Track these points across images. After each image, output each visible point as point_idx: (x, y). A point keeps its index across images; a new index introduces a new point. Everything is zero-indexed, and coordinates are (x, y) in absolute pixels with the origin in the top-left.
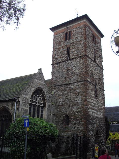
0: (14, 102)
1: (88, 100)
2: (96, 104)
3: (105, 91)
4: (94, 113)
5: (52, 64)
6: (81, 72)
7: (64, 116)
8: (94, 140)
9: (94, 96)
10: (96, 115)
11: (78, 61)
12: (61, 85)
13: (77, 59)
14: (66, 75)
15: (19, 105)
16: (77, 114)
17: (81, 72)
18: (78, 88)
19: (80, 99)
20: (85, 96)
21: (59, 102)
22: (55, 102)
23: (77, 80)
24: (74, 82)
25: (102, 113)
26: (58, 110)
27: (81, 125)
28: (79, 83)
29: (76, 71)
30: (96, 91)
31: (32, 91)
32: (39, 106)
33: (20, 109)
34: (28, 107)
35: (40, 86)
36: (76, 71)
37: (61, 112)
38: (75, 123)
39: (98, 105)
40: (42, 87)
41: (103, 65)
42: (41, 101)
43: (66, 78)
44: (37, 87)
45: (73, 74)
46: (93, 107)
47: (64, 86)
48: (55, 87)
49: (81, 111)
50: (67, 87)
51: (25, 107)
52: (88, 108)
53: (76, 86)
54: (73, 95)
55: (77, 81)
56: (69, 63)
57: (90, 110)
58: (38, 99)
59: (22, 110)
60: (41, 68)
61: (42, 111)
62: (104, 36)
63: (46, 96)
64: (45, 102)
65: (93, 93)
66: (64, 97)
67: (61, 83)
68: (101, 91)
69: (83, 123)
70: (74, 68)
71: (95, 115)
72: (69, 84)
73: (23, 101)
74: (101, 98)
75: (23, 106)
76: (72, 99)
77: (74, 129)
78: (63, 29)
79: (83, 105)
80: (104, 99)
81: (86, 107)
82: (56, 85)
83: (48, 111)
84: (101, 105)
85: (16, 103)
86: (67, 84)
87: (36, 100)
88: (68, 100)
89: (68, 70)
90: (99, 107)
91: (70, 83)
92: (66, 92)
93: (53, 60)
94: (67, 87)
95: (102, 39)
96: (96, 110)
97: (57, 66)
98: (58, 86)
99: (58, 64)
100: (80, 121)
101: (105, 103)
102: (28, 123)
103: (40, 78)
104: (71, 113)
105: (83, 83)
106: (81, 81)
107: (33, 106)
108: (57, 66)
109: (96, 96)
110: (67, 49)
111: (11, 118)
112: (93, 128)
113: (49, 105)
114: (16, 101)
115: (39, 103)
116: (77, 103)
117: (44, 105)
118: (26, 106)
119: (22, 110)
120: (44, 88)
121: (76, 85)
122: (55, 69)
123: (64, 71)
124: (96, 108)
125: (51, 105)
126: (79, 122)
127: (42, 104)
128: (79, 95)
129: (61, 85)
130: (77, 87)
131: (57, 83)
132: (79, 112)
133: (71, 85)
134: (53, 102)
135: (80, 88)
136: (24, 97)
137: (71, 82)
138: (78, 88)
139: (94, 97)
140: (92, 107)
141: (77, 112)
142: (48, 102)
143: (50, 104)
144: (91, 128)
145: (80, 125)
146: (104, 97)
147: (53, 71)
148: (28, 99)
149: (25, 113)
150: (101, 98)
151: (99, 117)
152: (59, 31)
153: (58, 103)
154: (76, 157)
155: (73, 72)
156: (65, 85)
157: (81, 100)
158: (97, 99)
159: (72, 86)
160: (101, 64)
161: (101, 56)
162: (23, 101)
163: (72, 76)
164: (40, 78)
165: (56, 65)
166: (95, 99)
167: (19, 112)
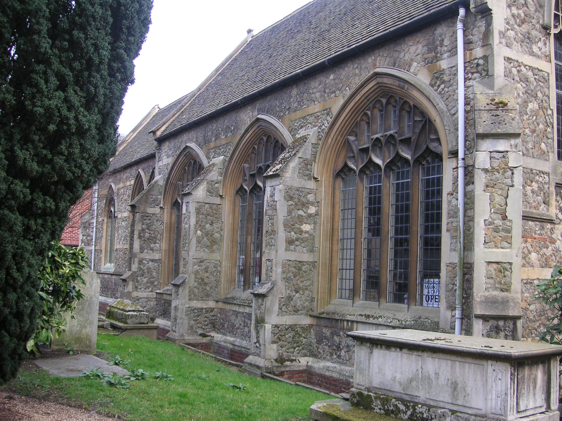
0: (441, 30)
15: (487, 35)
51: (532, 54)
59: (514, 71)
85: (460, 25)
111: (433, 146)
114: (462, 12)
118: (535, 49)
119: (514, 71)
149: (536, 97)
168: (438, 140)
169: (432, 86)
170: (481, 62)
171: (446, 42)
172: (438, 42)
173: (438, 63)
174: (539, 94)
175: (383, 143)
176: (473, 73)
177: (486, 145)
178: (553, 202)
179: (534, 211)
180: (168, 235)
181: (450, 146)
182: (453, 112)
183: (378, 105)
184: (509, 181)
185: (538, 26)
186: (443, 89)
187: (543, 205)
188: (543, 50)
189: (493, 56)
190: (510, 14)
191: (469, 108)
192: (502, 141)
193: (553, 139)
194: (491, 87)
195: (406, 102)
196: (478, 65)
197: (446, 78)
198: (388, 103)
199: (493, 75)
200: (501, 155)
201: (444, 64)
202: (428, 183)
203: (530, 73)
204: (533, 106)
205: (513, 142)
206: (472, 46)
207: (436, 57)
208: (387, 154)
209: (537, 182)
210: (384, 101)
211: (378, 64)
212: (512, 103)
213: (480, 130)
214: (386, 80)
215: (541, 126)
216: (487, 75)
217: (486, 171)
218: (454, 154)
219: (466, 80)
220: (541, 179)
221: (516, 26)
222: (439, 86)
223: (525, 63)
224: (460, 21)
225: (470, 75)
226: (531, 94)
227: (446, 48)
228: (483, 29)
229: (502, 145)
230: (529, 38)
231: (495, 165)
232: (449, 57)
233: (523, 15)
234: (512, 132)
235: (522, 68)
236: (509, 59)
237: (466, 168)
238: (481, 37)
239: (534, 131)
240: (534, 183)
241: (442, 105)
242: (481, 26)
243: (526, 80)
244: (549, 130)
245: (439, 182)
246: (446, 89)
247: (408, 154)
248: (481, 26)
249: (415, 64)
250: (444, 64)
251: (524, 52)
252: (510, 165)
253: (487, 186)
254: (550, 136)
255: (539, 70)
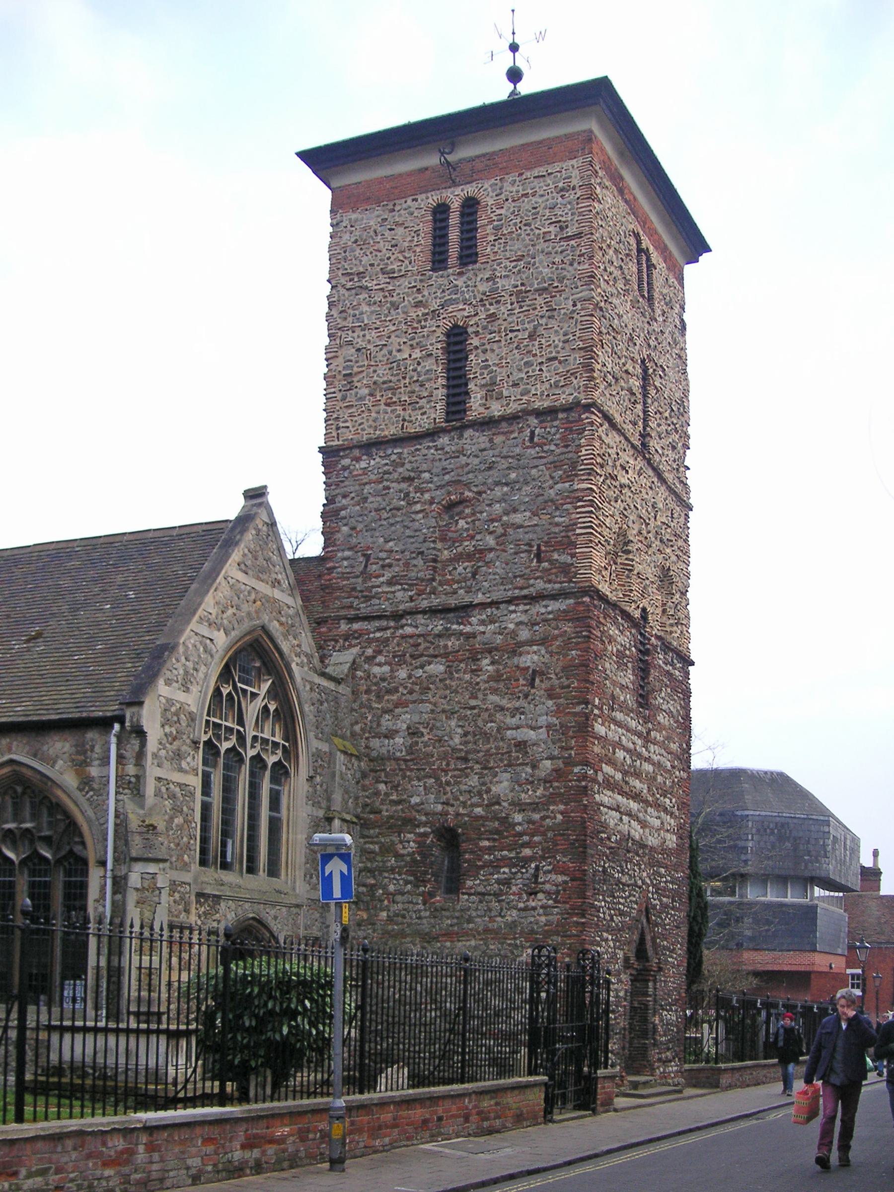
0: (91, 735)
1: (600, 729)
2: (639, 756)
3: (692, 663)
4: (629, 814)
5: (321, 450)
6: (557, 530)
7: (425, 835)
8: (622, 994)
9: (628, 698)
10: (637, 832)
11: (534, 445)
12: (402, 617)
13: (528, 432)
14: (439, 545)
15: (140, 755)
16: (518, 818)
17: (557, 530)
18: (530, 643)
19: (543, 720)
20: (579, 704)
21: (390, 735)
22: (353, 734)
23: (520, 582)
24: (495, 596)
25: (672, 814)
26: (377, 793)
27: (548, 893)
28: (539, 608)
29: (517, 518)
30: (643, 669)
31: (217, 657)
32: (258, 760)
33: (150, 788)
34: (195, 771)
35: (265, 618)
36: (517, 518)
37: (399, 802)
38: (507, 882)
39: (648, 760)
40: (275, 627)
41: (692, 478)
42: (268, 727)
43: (435, 561)
44: (246, 626)
45: (491, 541)
46: (625, 773)
47: (421, 619)
48: (356, 626)
49: (552, 799)
50: (447, 629)
51: (181, 770)
52: (595, 780)
53: (518, 624)
54: (495, 691)
55: (525, 592)
56: (461, 452)
57: (605, 797)
58: (252, 710)
59: (163, 789)
60: (265, 487)
61: (275, 803)
62: (708, 249)
63: (301, 688)
64: (290, 734)
65: (628, 677)
66: (422, 701)
67: (399, 595)
68: (672, 664)
69: (560, 878)
70: (498, 492)
71: (633, 832)
72: (464, 610)
73: (167, 729)
74: (670, 714)
75: (167, 764)
76: (485, 715)
77: (499, 919)
78: (410, 174)
79: (566, 764)
80: (687, 718)
81: (585, 777)
82: (364, 609)
83: (313, 800)
84: (669, 767)
85: (114, 740)
86: (444, 611)
87: (241, 722)
88: (453, 723)
89: (450, 507)
90: (655, 779)
91: (471, 606)
92: (437, 668)
93: (332, 419)
94: (446, 634)
95: (689, 271)
96: (636, 796)
97: (363, 464)
98: (379, 618)
99: (370, 456)
100: (537, 868)
101: (689, 747)
102: (345, 879)
103: (261, 561)
104: (479, 810)
105: (564, 611)
106: (554, 597)
107: (221, 761)
108: (363, 464)
109: (644, 699)
110: (448, 344)
111: (77, 849)
112: (622, 913)
113: (318, 755)
114: (117, 727)
115: (255, 738)
116: (522, 745)
117: (290, 753)
118: (184, 765)
119: (163, 789)
120: (285, 636)
121: (514, 617)
122: (351, 487)
123: (418, 507)
124: (637, 784)
125: (331, 754)
126: (536, 876)
127: (276, 745)
128: (538, 694)
129: (397, 616)
130: (524, 634)
131: (368, 598)
132: (535, 806)
133: (474, 620)
134: (343, 737)
135: (544, 641)
136: (170, 702)
137: (480, 598)
138: (530, 643)
139: (628, 711)
140: (619, 776)
141: (521, 807)
142: (311, 735)
143: (325, 747)
144: (611, 916)
145: (540, 896)
146: (687, 708)
147: (330, 500)
148: (192, 718)
149: (181, 812)
150: (670, 714)
151: (652, 841)
152: (380, 181)
153: (375, 743)
154: (546, 1084)
155: (493, 521)
156: (433, 612)
157: (549, 727)
158: (647, 720)
159: (482, 623)
160: (681, 467)
161: (681, 408)
162: (167, 729)
163: (481, 552)
164: (261, 561)
165: (358, 459)
166: (633, 724)
167: (142, 807)
168: (83, 843)
169: (81, 790)
170: (133, 780)
171: (97, 749)
172: (88, 747)
173: (88, 768)
174: (185, 809)
175: (18, 837)
176: (124, 789)
177: (138, 867)
178: (193, 911)
179: (176, 919)
180: (94, 995)
181: (98, 854)
182: (102, 821)
183: (10, 792)
184: (156, 899)
185: (188, 741)
186: (92, 797)
187: (184, 913)
188: (192, 765)
189: (145, 777)
190: (163, 733)
191: (118, 821)
192: (152, 864)
193: (195, 850)
194: (142, 807)
195: (46, 797)
196: (130, 782)
197: (96, 786)
198: (24, 793)
199: (144, 796)
200: (151, 876)
201: (94, 771)
202: (68, 885)
203: (178, 789)
204: (179, 820)
205: (161, 865)
206: (125, 761)
207: (85, 761)
208: (21, 849)
209: (179, 892)
210: (19, 789)
211: (252, 1094)
212: (161, 826)
213: (134, 854)
214: (24, 770)
215: (185, 839)
216: (138, 793)
217: (137, 889)
218: (103, 863)
219: (117, 793)
220: (182, 889)
221: (167, 745)
222: (87, 793)
223: (174, 780)
224: (115, 735)
225: (121, 790)
226: (177, 810)
227: (96, 756)
228: (137, 748)
229: (152, 868)
230: (178, 755)
231: (146, 885)
232: (100, 765)
233: (175, 732)
234: (161, 857)
235: (171, 786)
236: (159, 778)
237: (114, 878)
238: (134, 755)
239: (178, 845)
240: (176, 894)
241: (90, 813)
242: (134, 744)
243: (173, 796)
244: (192, 842)
245: (84, 886)
246: (95, 797)
247: (47, 852)
248: (134, 744)
249: (60, 762)
250: (94, 771)
251: (174, 770)
252: (159, 885)
253: (138, 903)
254: (192, 848)
255: (187, 785)
